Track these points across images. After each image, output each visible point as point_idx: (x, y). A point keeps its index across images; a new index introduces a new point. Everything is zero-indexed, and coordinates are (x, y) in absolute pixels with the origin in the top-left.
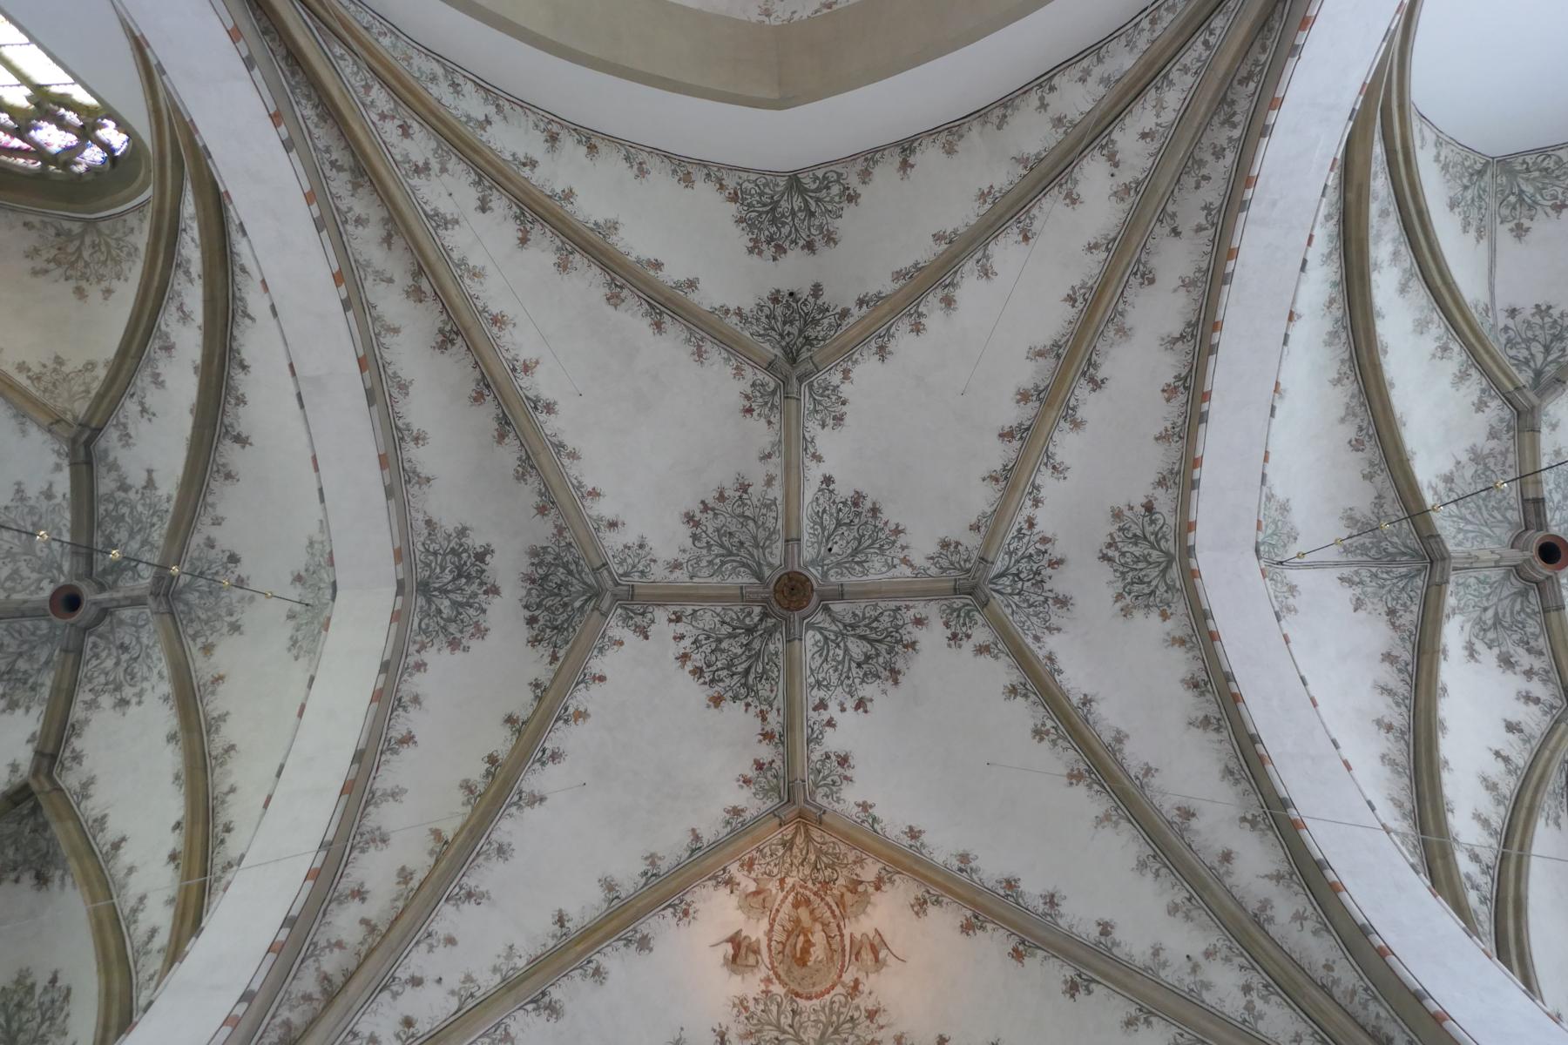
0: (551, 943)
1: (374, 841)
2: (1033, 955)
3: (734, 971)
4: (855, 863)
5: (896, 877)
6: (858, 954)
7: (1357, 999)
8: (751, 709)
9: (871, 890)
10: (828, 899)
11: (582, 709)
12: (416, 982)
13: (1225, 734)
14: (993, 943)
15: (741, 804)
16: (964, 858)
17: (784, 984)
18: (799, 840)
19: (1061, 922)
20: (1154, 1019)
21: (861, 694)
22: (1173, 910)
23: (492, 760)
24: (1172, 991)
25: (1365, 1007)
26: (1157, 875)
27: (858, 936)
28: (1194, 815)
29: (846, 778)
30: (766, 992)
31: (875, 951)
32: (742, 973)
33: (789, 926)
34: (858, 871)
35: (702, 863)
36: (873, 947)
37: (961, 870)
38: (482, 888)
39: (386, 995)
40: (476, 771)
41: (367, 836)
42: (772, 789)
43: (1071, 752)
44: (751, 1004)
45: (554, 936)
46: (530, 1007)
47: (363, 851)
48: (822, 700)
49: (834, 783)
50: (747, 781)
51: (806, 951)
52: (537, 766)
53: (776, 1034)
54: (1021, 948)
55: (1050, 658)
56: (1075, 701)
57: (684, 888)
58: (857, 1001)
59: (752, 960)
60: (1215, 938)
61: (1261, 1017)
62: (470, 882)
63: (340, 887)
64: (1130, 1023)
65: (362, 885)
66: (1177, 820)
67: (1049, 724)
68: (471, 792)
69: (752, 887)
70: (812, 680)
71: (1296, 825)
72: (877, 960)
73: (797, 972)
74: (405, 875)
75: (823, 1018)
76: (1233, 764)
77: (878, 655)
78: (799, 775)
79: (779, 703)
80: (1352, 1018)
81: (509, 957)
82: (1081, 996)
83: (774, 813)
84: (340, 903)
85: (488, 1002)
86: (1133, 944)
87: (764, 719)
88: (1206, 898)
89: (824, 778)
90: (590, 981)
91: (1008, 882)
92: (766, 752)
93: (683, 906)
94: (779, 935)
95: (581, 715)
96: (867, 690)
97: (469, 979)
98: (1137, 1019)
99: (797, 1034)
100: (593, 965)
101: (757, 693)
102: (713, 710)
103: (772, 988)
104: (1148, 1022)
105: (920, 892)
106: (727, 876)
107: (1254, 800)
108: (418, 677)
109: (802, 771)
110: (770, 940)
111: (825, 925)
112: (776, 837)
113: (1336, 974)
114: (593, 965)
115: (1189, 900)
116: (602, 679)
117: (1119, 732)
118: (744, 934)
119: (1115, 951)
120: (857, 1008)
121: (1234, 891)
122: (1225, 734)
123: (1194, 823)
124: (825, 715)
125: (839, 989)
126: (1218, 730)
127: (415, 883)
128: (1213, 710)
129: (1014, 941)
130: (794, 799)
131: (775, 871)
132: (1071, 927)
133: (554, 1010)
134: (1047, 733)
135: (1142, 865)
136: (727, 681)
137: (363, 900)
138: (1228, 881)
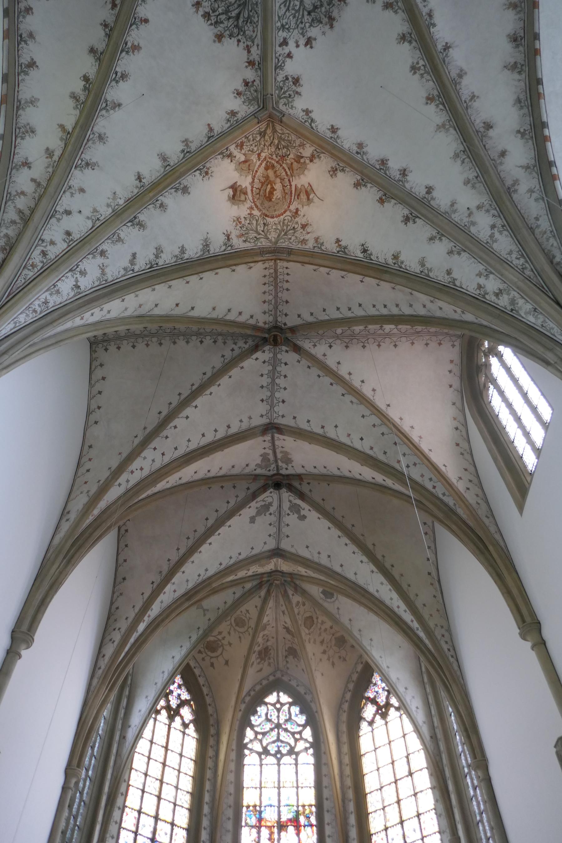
0: (136, 191)
1: (27, 132)
2: (389, 202)
3: (233, 204)
4: (300, 146)
5: (322, 155)
6: (299, 195)
7: (545, 236)
8: (241, 44)
9: (308, 161)
10: (284, 165)
11: (136, 44)
12: (68, 213)
13: (523, 76)
14: (370, 194)
15: (236, 108)
16: (360, 145)
17: (260, 210)
18: (269, 131)
19: (407, 185)
20: (443, 238)
21: (309, 34)
22: (467, 182)
23: (86, 79)
24: (456, 225)
25: (548, 240)
26: (463, 162)
27: (299, 186)
28: (492, 127)
29: (297, 93)
30: (250, 214)
31: (308, 194)
32: (238, 205)
33: (263, 180)
34: (301, 151)
35: (214, 144)
36: (306, 192)
37: (357, 153)
38: (94, 160)
39: (53, 220)
40: (78, 86)
41: (23, 130)
42: (254, 99)
43: (431, 83)
44: (243, 220)
45: (137, 187)
46: (129, 224)
47: (23, 138)
48: (285, 39)
49: (290, 96)
50: (239, 94)
51: (271, 193)
52: (114, 83)
53: (255, 235)
54: (384, 198)
55: (430, 15)
56: (440, 47)
57: (206, 158)
58: (297, 219)
59: (243, 198)
60: (484, 199)
61: (496, 241)
62: (87, 156)
63: (15, 160)
64: (432, 239)
65: (27, 159)
66: (482, 130)
67: (421, 63)
68: (77, 100)
69: (243, 158)
70: (279, 24)
71: (546, 139)
72: (308, 199)
73: (267, 204)
74: (49, 153)
75: (279, 228)
76: (522, 97)
77: (322, 6)
78: (269, 91)
79: (258, 41)
80: (540, 244)
82: (410, 224)
83: (254, 115)
84: (18, 170)
85: (107, 223)
86: (441, 200)
87: (249, 52)
88: (485, 177)
89: (284, 93)
90: (158, 210)
91: (382, 161)
92: (250, 74)
93: (205, 169)
94: (257, 185)
95: (136, 48)
96: (314, 32)
97: (95, 211)
98: (435, 237)
99: (266, 235)
100: (159, 202)
101: (244, 33)
102: (217, 44)
103: (253, 212)
104: (440, 239)
105: (334, 164)
106: (228, 152)
107: (528, 119)
108: (29, 18)
109: (272, 89)
110: (252, 187)
111: (282, 180)
112: (256, 129)
113: (539, 223)
114: (159, 202)
115: (477, 177)
116: (146, 21)
117: (461, 70)
118: (238, 184)
119: (432, 203)
120: (297, 223)
121: (501, 174)
122: (523, 76)
123: (491, 133)
124: (286, 50)
125: (288, 213)
126: (520, 73)
127: (56, 158)
128: (520, 58)
129: (380, 194)
130: (266, 104)
131: (255, 149)
132: (411, 188)
133: (141, 225)
134: (419, 69)
135: (456, 155)
136: (226, 22)
137: (30, 168)
138: (500, 168)
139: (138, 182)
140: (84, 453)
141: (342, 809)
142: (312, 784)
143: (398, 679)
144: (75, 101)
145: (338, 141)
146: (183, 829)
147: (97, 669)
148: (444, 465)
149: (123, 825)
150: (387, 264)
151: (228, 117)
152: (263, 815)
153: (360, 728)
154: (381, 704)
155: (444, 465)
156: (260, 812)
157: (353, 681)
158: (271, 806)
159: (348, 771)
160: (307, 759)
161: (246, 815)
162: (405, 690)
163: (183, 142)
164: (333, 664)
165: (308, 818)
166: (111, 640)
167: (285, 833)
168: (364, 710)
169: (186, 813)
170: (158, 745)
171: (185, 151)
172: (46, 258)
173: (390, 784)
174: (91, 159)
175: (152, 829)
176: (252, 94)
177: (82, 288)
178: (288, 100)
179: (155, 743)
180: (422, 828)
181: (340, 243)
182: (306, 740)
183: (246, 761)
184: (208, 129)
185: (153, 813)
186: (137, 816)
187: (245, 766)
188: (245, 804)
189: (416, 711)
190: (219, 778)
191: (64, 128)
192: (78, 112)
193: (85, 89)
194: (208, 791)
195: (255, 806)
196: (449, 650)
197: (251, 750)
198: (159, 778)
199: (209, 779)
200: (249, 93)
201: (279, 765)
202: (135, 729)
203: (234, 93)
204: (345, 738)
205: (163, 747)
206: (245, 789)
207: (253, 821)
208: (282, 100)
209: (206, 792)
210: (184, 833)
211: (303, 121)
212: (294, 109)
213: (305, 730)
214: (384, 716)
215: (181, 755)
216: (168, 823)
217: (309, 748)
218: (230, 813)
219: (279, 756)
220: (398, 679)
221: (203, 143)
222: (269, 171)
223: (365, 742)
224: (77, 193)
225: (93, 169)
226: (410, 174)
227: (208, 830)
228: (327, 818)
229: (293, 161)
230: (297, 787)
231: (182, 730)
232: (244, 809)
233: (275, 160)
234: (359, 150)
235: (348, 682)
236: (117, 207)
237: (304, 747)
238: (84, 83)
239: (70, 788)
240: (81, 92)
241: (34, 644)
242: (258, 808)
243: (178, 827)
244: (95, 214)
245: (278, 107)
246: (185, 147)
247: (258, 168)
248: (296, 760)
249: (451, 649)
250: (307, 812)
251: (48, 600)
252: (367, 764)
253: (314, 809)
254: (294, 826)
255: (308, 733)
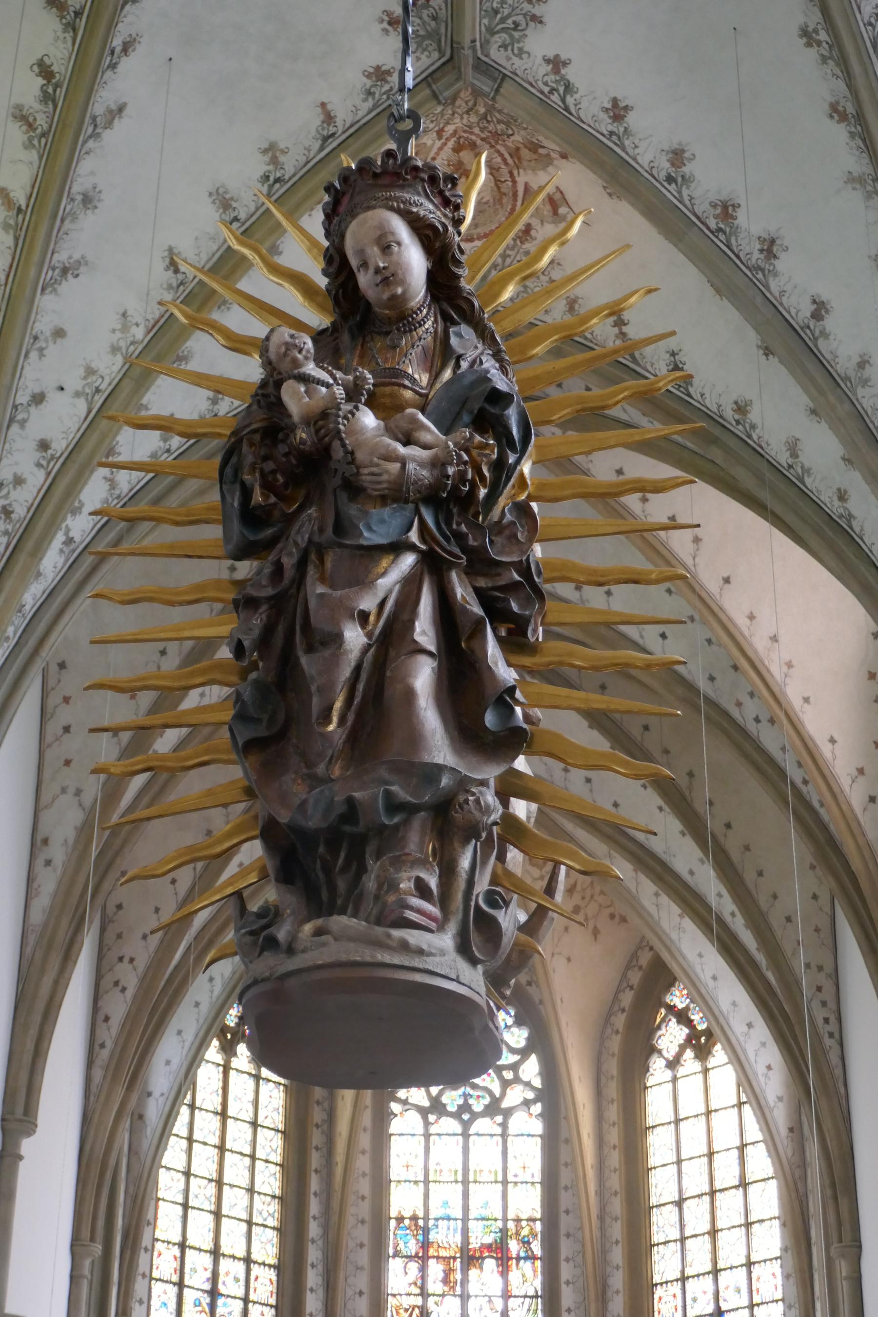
12: (38, 399)
23: (45, 71)
38: (77, 256)
39: (15, 428)
40: (29, 88)
42: (429, 36)
49: (516, 25)
62: (61, 257)
68: (31, 126)
81: (125, 329)
91: (725, 207)
97: (90, 371)
119: (821, 343)
139: (170, 273)
140: (51, 683)
141: (596, 1232)
142: (538, 1178)
143: (734, 1004)
144: (24, 128)
145: (627, 143)
146: (270, 1266)
147: (97, 1048)
148: (832, 741)
149: (155, 1274)
150: (721, 417)
151: (369, 83)
152: (432, 1237)
153: (648, 1070)
154: (699, 1028)
155: (832, 741)
156: (426, 1231)
157: (640, 968)
158: (449, 1219)
159: (615, 1159)
160: (529, 1124)
161: (395, 1234)
162: (746, 1029)
163: (265, 152)
164: (596, 933)
165: (526, 1243)
166: (116, 983)
167: (478, 1271)
168: (659, 1033)
169: (272, 1236)
170: (207, 1111)
171: (272, 179)
172: (11, 521)
173: (699, 1196)
174: (70, 258)
175: (209, 1274)
176: (424, 23)
177: (77, 539)
178: (511, 37)
179: (201, 1109)
180: (754, 1288)
181: (625, 329)
182: (528, 1084)
183: (395, 1126)
184: (322, 117)
185: (209, 1245)
186: (178, 1254)
187: (392, 1138)
188: (393, 1213)
189: (766, 1076)
190: (339, 1170)
191: (7, 196)
192: (34, 155)
193: (47, 98)
194: (315, 1194)
195: (414, 1218)
196: (826, 1021)
197: (405, 1102)
198: (215, 1176)
199: (316, 1171)
200: (418, 21)
201: (466, 1135)
202: (161, 1100)
203: (382, 21)
204: (613, 1090)
205: (216, 1113)
206: (393, 1185)
207: (412, 1246)
208: (496, 38)
209: (312, 1197)
210: (272, 1274)
211: (546, 90)
212: (525, 56)
213: (527, 1062)
214: (703, 1053)
215: (255, 1124)
216: (239, 1259)
217: (535, 1101)
218: (363, 1234)
219: (466, 1117)
220: (734, 1004)
221: (312, 155)
222: (462, 154)
223: (657, 1104)
224: (51, 344)
225: (77, 276)
226: (782, 255)
227: (320, 1268)
228: (566, 1248)
229: (521, 146)
230: (505, 1182)
231: (254, 1072)
232: (393, 1223)
233: (477, 135)
234: (672, 170)
235: (628, 967)
236: (132, 348)
237: (522, 1100)
238: (41, 81)
239: (83, 1276)
240: (37, 106)
241: (38, 1129)
242: (421, 1223)
243: (260, 1264)
244: (89, 380)
245: (487, 56)
246: (271, 167)
247: (437, 154)
248: (504, 1125)
249: (833, 1019)
250: (525, 1232)
251: (45, 1044)
252: (659, 1147)
253: (538, 1226)
254: (497, 1259)
255: (531, 1069)
